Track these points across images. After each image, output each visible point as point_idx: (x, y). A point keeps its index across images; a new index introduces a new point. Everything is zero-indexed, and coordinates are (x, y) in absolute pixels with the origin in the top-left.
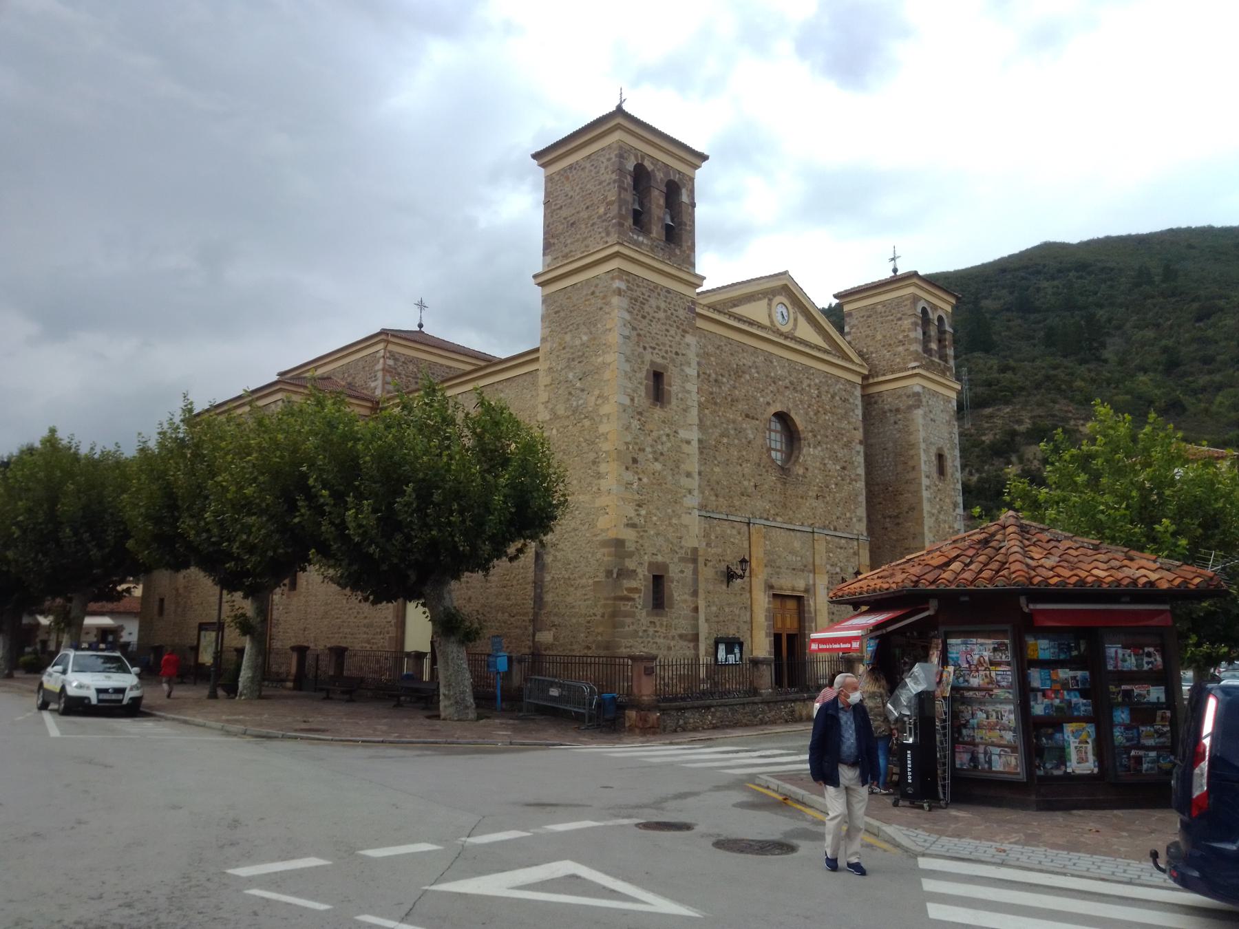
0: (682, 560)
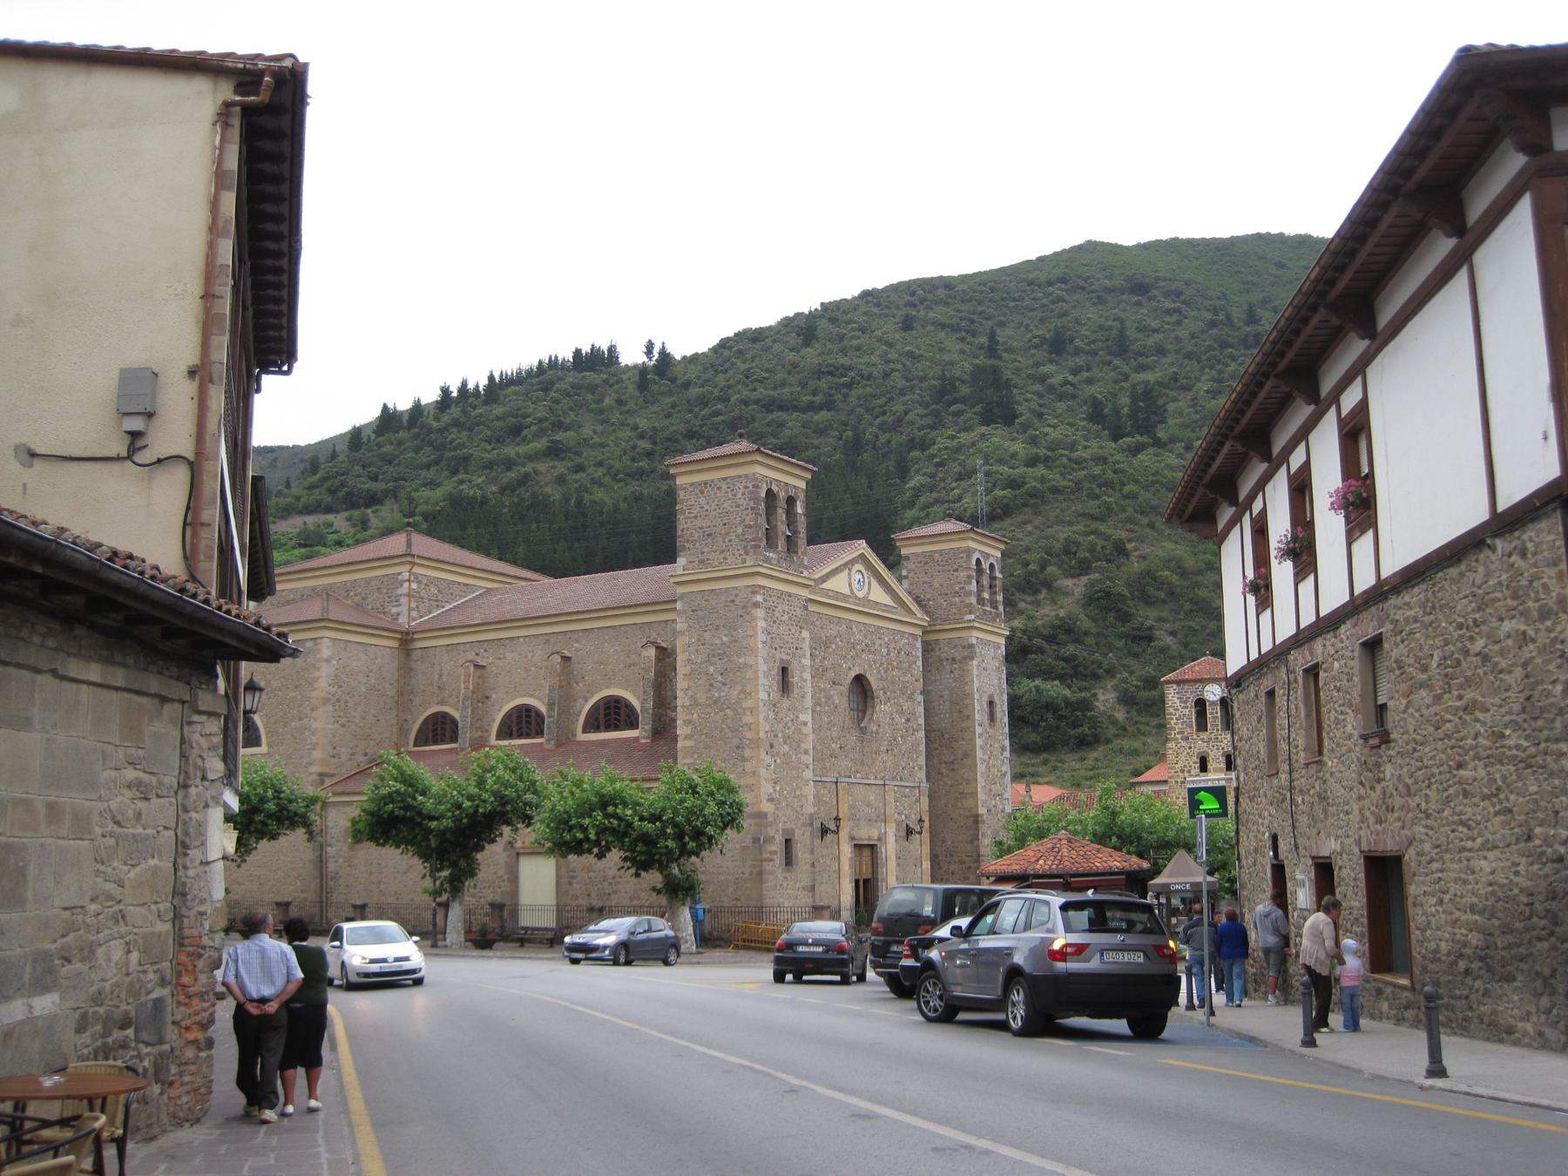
0: (804, 825)
